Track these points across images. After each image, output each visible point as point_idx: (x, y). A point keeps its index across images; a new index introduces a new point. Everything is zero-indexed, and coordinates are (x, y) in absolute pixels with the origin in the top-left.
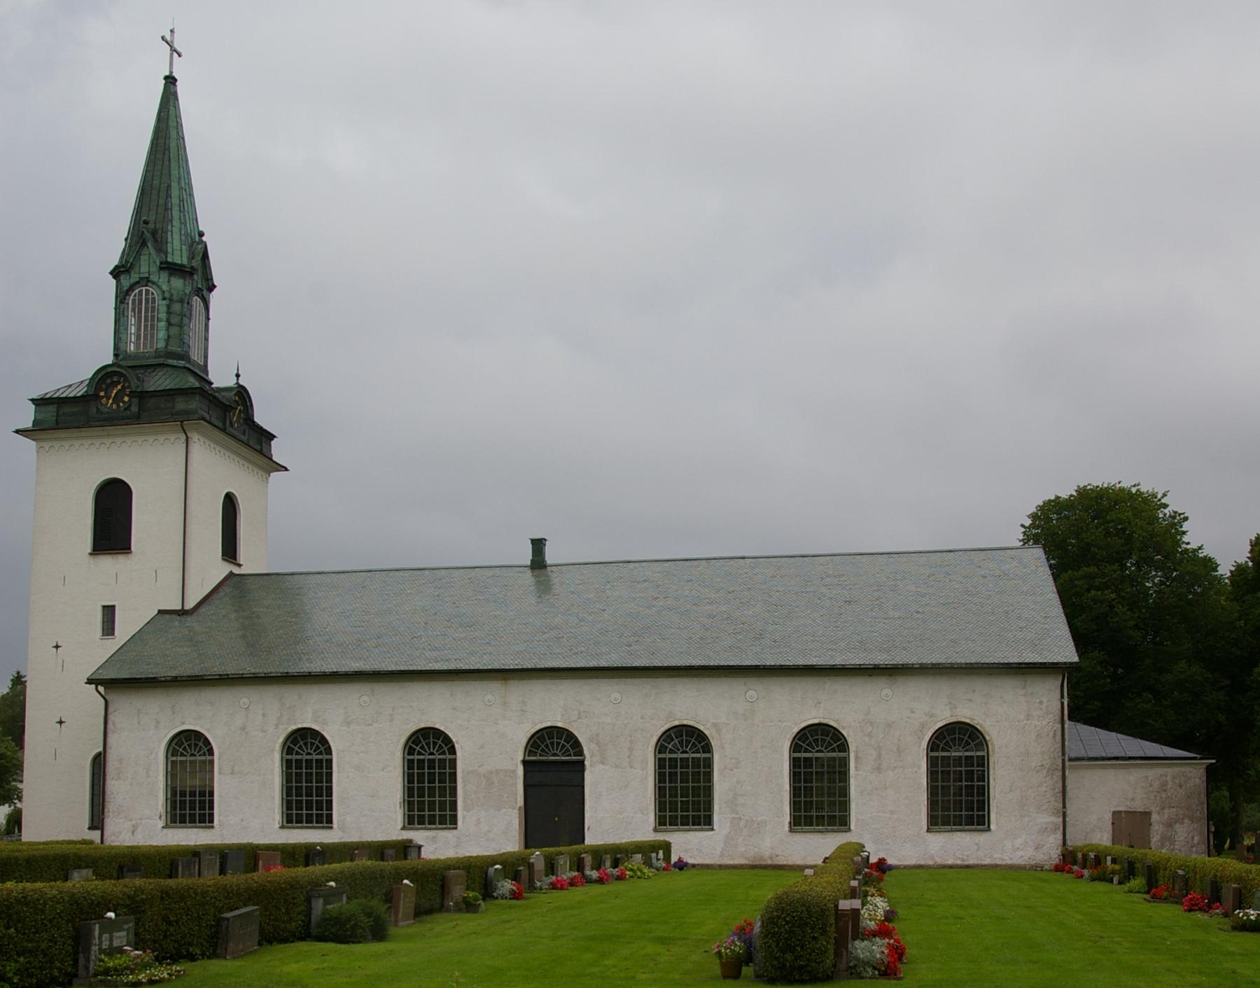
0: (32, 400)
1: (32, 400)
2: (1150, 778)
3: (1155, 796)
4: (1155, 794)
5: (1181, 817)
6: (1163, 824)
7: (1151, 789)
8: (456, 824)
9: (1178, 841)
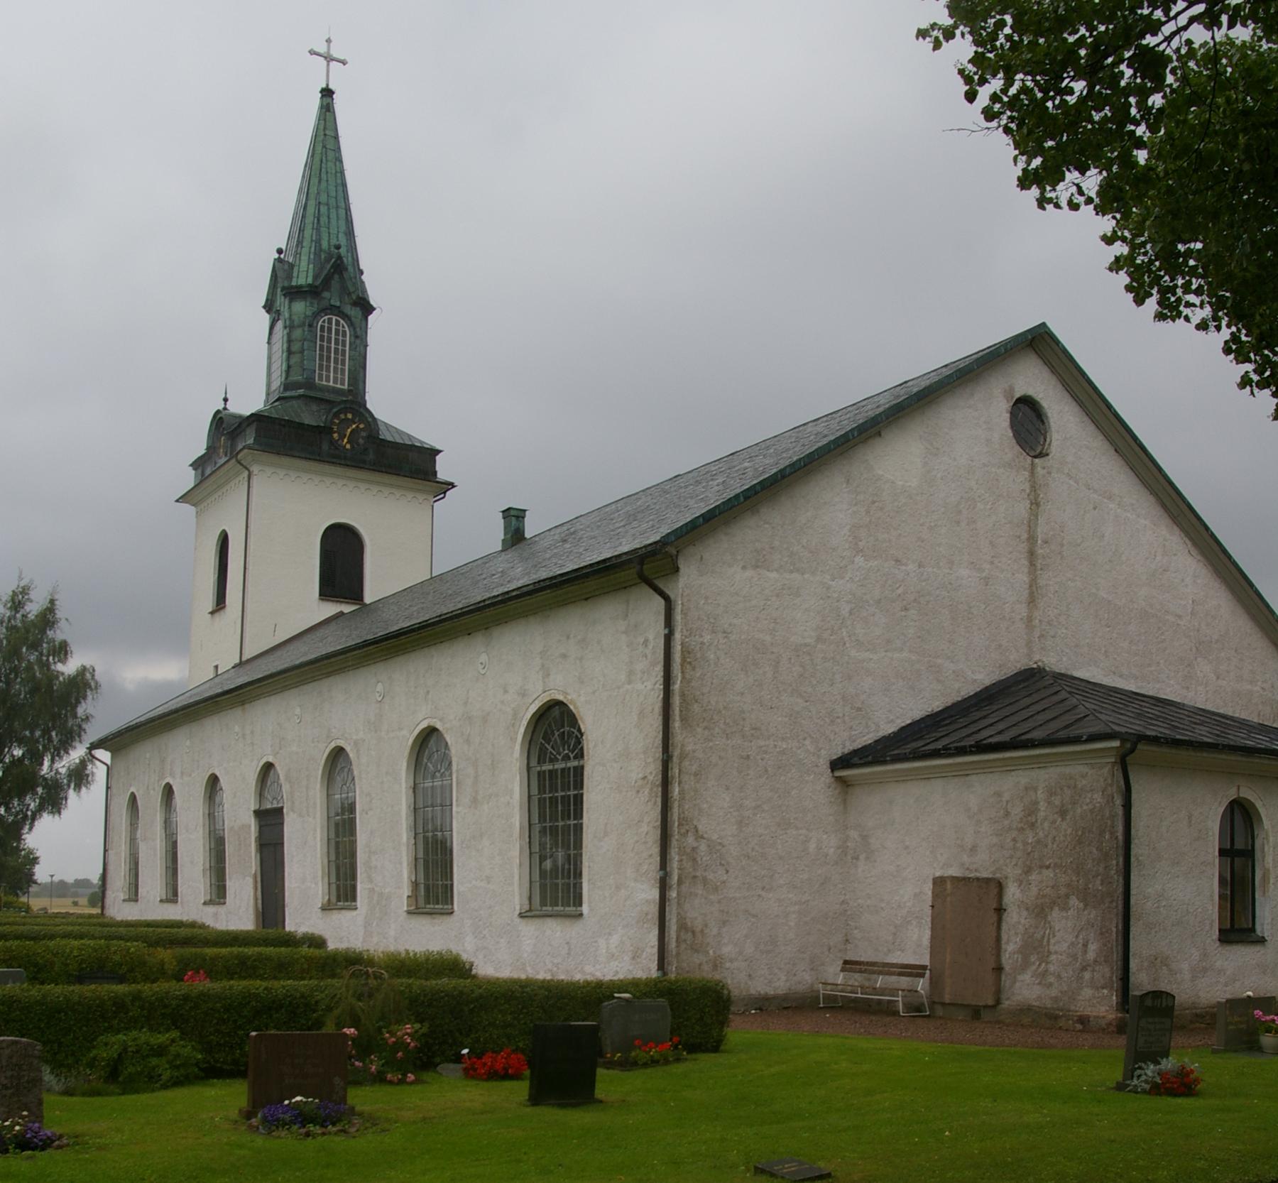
0: (441, 451)
1: (441, 451)
2: (1006, 796)
3: (1014, 840)
4: (1015, 833)
5: (1063, 891)
6: (1027, 909)
7: (1006, 822)
8: (224, 897)
9: (1056, 953)
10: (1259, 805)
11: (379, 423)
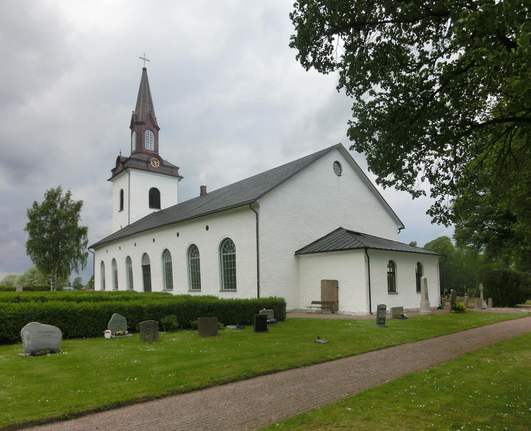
10: (395, 261)
11: (164, 161)
